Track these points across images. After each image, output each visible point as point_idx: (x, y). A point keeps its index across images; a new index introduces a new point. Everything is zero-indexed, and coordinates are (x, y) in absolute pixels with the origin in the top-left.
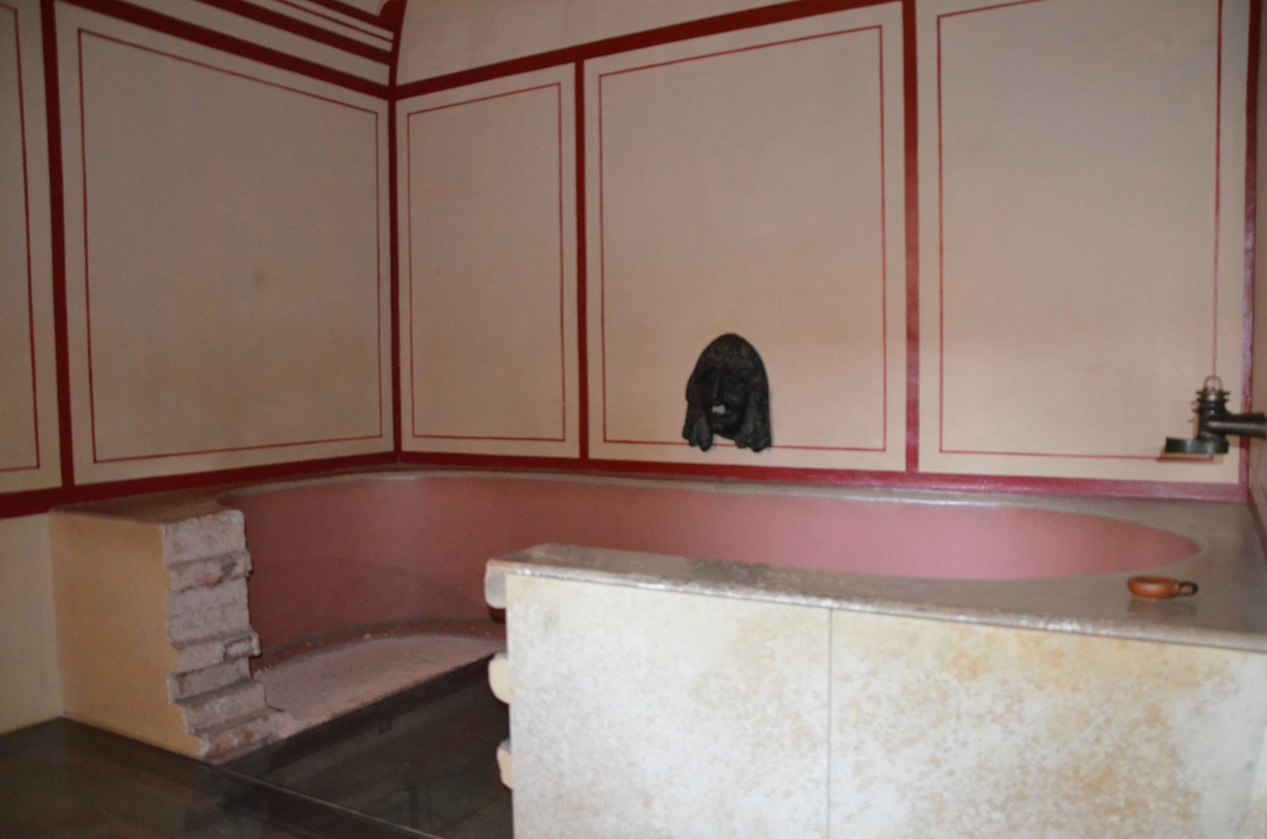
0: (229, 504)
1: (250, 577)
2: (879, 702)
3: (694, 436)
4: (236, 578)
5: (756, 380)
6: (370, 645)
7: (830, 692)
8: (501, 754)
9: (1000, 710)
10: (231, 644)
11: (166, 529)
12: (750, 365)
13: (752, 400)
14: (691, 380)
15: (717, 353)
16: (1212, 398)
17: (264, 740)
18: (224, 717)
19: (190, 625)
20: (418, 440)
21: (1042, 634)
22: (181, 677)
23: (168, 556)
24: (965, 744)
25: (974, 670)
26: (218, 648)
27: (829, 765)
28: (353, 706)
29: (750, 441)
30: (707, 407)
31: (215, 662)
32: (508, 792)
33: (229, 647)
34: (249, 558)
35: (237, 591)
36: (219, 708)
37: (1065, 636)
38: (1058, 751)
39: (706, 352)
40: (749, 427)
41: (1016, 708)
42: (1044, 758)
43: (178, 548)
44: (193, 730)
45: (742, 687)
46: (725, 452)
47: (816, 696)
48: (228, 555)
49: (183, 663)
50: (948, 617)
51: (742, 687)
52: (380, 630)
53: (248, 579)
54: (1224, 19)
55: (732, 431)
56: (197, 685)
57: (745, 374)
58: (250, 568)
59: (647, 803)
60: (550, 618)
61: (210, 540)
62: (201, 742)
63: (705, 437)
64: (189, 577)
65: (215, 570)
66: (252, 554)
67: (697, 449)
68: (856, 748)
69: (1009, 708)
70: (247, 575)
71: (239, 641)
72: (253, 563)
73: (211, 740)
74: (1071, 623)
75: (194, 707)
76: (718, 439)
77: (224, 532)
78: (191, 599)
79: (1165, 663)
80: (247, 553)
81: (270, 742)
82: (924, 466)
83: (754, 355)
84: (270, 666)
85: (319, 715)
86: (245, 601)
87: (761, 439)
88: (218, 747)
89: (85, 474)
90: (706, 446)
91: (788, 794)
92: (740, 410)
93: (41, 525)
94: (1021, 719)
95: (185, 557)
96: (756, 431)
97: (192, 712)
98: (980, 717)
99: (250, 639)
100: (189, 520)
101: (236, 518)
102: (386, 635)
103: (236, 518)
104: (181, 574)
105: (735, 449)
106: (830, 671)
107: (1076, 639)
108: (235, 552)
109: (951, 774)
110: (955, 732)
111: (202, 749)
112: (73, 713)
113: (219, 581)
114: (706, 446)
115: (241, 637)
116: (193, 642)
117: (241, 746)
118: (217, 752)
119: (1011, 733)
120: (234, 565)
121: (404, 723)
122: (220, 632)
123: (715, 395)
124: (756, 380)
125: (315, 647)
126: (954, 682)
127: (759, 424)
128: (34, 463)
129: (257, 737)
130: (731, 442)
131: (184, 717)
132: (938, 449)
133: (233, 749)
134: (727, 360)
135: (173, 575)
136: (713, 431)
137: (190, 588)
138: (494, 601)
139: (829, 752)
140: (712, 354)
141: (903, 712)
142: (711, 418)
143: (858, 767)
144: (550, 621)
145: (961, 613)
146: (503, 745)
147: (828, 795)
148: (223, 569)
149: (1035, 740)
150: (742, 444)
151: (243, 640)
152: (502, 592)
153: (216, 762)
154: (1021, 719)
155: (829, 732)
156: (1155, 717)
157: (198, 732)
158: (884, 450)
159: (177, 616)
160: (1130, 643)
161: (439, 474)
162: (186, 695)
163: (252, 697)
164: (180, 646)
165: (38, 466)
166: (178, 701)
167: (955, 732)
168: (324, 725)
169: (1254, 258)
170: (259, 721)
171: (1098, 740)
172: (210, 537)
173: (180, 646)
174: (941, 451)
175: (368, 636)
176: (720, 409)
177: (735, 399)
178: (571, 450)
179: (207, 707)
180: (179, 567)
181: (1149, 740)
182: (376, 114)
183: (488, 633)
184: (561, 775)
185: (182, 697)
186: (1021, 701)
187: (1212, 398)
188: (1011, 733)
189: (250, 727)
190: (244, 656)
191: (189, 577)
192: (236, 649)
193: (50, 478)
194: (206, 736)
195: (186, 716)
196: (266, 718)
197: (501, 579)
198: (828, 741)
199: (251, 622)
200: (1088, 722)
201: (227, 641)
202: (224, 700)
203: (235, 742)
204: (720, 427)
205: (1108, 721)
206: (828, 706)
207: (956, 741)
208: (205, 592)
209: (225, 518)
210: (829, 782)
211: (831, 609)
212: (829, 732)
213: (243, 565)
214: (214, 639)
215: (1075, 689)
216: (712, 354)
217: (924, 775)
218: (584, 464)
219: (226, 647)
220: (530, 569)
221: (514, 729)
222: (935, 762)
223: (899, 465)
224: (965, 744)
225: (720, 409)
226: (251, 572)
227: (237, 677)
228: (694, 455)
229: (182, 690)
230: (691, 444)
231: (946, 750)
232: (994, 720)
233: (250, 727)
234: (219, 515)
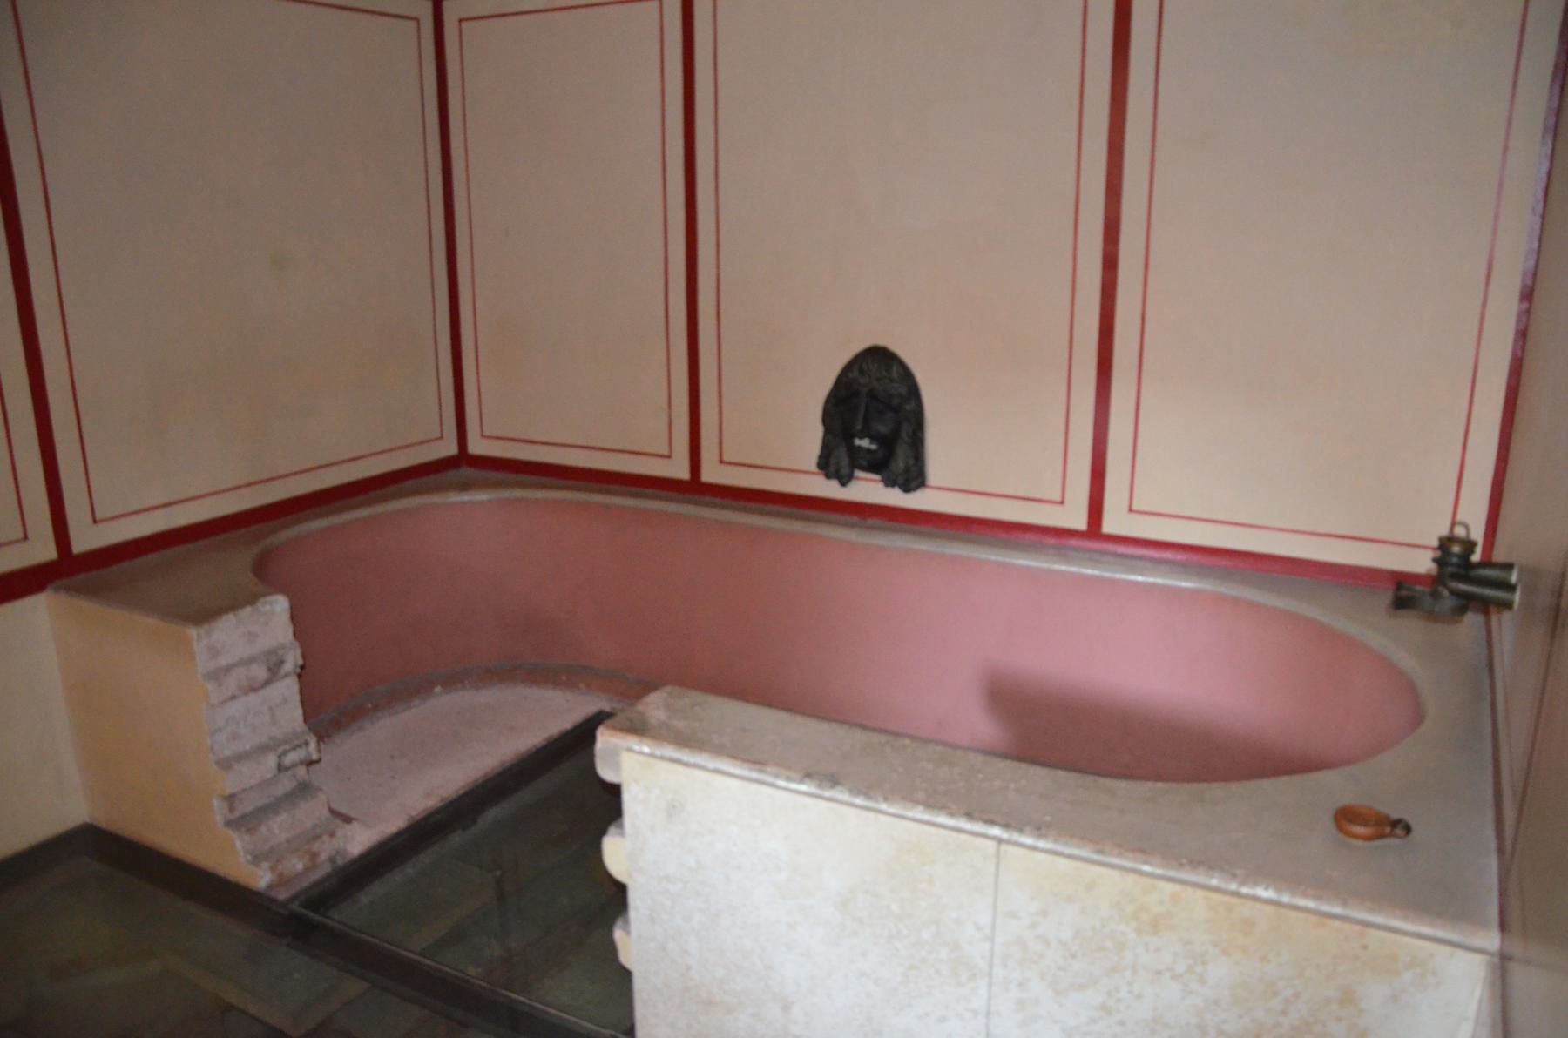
0: (266, 574)
1: (302, 673)
2: (1048, 944)
3: (832, 469)
4: (286, 675)
5: (908, 407)
6: (443, 703)
7: (994, 926)
8: (618, 934)
9: (1181, 968)
10: (285, 753)
11: (199, 635)
12: (903, 390)
13: (904, 435)
14: (827, 401)
15: (861, 371)
16: (1456, 549)
17: (332, 860)
18: (284, 836)
19: (235, 737)
20: (414, 14)
21: (1234, 900)
22: (231, 799)
23: (203, 663)
24: (1139, 996)
25: (1156, 925)
26: (271, 760)
27: (990, 998)
28: (432, 803)
29: (900, 480)
30: (848, 436)
31: (269, 776)
32: (626, 975)
33: (283, 757)
34: (298, 652)
35: (288, 688)
36: (278, 829)
37: (1258, 905)
38: (1240, 1017)
39: (848, 368)
40: (900, 463)
41: (1199, 969)
42: (1224, 1022)
43: (214, 652)
44: (249, 857)
45: (895, 908)
46: (868, 489)
47: (978, 928)
48: (272, 652)
49: (230, 784)
50: (1129, 864)
51: (895, 908)
52: (452, 681)
53: (299, 676)
54: (1525, 55)
55: (878, 465)
56: (245, 807)
57: (896, 401)
58: (300, 662)
59: (786, 1008)
60: (674, 807)
61: (252, 637)
62: (261, 873)
63: (845, 471)
64: (231, 683)
65: (260, 672)
66: (302, 646)
67: (834, 484)
68: (1020, 985)
69: (1190, 969)
70: (298, 670)
71: (294, 748)
72: (304, 656)
73: (272, 869)
74: (1266, 889)
75: (249, 831)
76: (859, 473)
77: (267, 624)
78: (235, 708)
79: (1365, 947)
80: (297, 644)
81: (340, 862)
82: (1107, 528)
83: (908, 376)
84: (326, 739)
85: (392, 822)
86: (297, 697)
87: (913, 479)
88: (281, 875)
89: (85, 539)
90: (844, 481)
91: (943, 1020)
92: (888, 444)
93: (38, 608)
94: (1202, 981)
95: (223, 661)
96: (907, 470)
97: (247, 838)
98: (1159, 973)
99: (307, 743)
100: (225, 617)
101: (279, 605)
102: (459, 686)
103: (279, 605)
104: (220, 685)
105: (881, 486)
106: (995, 905)
107: (1270, 909)
108: (283, 646)
109: (1122, 1023)
110: (1130, 984)
111: (261, 879)
112: (103, 822)
113: (267, 683)
114: (844, 481)
115: (296, 742)
116: (241, 757)
117: (307, 870)
118: (282, 881)
119: (1191, 992)
120: (282, 662)
121: (491, 815)
122: (271, 738)
123: (859, 427)
124: (908, 407)
125: (376, 708)
126: (1132, 935)
127: (912, 462)
128: (20, 535)
129: (323, 856)
130: (877, 477)
131: (238, 844)
132: (1127, 508)
133: (299, 876)
134: (875, 383)
135: (210, 686)
136: (855, 465)
137: (233, 697)
138: (606, 773)
139: (990, 985)
140: (855, 374)
141: (1073, 956)
142: (854, 452)
143: (1021, 1005)
144: (674, 810)
145: (1145, 862)
146: (619, 923)
147: (987, 1026)
148: (269, 669)
149: (1217, 1002)
150: (890, 482)
151: (299, 746)
152: (617, 767)
153: (283, 895)
154: (1202, 981)
155: (991, 966)
156: (1348, 998)
157: (257, 859)
158: (1062, 503)
159: (220, 730)
160: (1330, 922)
161: (518, 493)
162: (237, 814)
163: (311, 812)
164: (226, 764)
165: (26, 538)
166: (229, 824)
167: (1130, 984)
168: (399, 834)
169: (1528, 312)
170: (325, 838)
171: (1284, 1012)
172: (250, 633)
173: (226, 764)
174: (1131, 510)
175: (438, 689)
176: (864, 443)
177: (883, 429)
178: (679, 470)
179: (263, 829)
180: (217, 675)
181: (1339, 1019)
182: (417, 20)
183: (582, 685)
184: (688, 968)
185: (232, 817)
186: (1204, 963)
187: (1456, 549)
188: (1191, 992)
189: (316, 847)
190: (301, 763)
191: (231, 683)
192: (291, 758)
193: (43, 550)
194: (265, 865)
195: (240, 843)
196: (332, 835)
197: (614, 753)
198: (990, 975)
199: (305, 721)
200: (1276, 994)
201: (280, 750)
202: (283, 817)
203: (300, 867)
204: (865, 463)
205: (1297, 996)
206: (992, 940)
207: (1130, 992)
208: (252, 697)
209: (268, 607)
210: (988, 1014)
211: (1000, 841)
212: (991, 966)
213: (293, 659)
214: (264, 749)
215: (1264, 959)
216: (855, 374)
217: (1093, 1021)
218: (694, 488)
219: (280, 757)
220: (649, 746)
221: (633, 914)
222: (1106, 1009)
223: (1081, 524)
224: (1139, 996)
225: (864, 443)
226: (302, 667)
227: (294, 784)
228: (829, 489)
229: (231, 809)
230: (828, 476)
231: (1119, 1000)
232: (1174, 977)
233: (316, 847)
234: (259, 605)
